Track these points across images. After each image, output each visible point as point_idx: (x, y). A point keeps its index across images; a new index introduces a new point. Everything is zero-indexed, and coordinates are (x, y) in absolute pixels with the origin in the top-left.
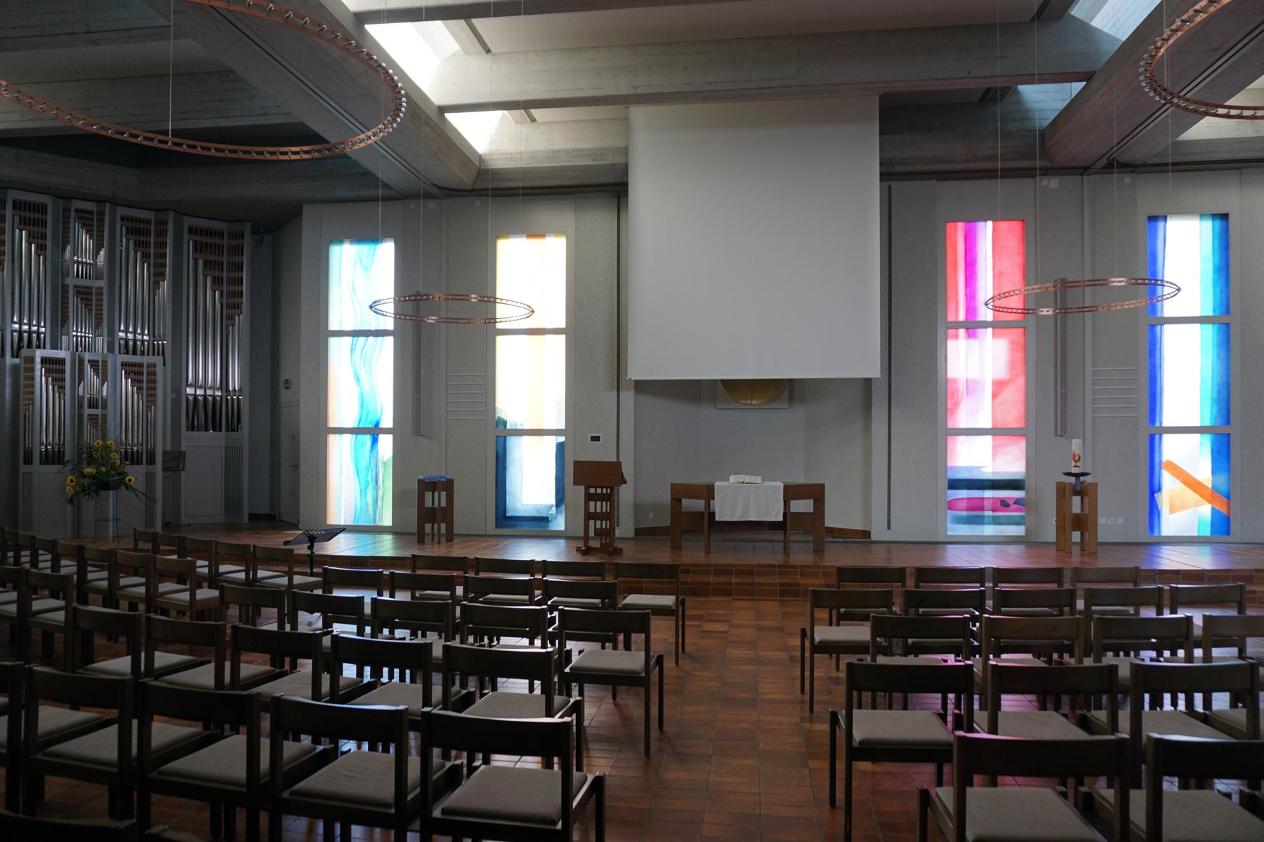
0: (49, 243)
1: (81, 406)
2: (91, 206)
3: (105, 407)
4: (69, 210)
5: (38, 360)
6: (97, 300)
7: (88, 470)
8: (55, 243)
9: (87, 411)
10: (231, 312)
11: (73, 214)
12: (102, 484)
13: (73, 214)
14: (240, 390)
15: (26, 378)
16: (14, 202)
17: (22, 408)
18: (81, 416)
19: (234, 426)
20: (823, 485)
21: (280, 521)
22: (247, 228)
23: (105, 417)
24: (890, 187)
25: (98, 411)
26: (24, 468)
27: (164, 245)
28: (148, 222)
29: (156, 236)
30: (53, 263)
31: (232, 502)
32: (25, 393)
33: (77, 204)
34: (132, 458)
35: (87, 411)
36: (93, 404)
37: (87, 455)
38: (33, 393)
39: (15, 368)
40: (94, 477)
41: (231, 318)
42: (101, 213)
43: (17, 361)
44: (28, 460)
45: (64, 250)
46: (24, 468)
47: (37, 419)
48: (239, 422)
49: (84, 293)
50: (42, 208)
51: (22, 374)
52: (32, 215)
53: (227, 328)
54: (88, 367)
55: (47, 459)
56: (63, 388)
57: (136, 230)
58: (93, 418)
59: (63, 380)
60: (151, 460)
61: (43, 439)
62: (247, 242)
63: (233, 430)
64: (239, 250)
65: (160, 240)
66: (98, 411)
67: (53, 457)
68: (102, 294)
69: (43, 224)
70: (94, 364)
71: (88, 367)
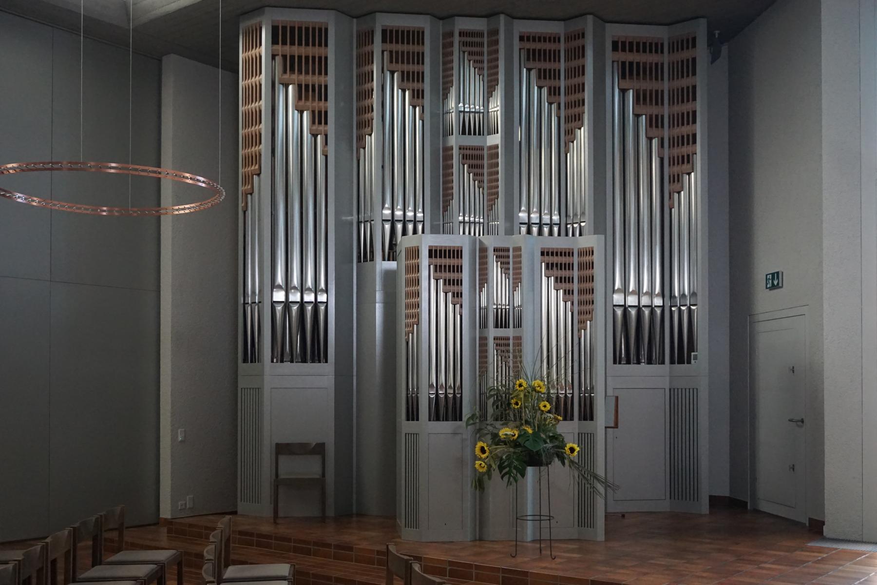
0: (427, 87)
1: (484, 325)
2: (479, 25)
3: (519, 325)
4: (451, 34)
5: (424, 253)
6: (490, 174)
7: (505, 432)
8: (434, 80)
9: (492, 332)
10: (676, 169)
11: (456, 39)
12: (529, 455)
13: (456, 39)
14: (693, 294)
15: (409, 295)
16: (384, 32)
17: (402, 329)
18: (483, 340)
19: (683, 353)
20: (277, 445)
21: (757, 511)
22: (701, 30)
23: (518, 339)
24: (127, 528)
25: (510, 332)
26: (406, 426)
27: (581, 71)
28: (555, 39)
29: (567, 59)
30: (433, 115)
31: (681, 476)
32: (408, 316)
33: (463, 24)
34: (563, 408)
35: (492, 332)
36: (501, 322)
37: (503, 405)
38: (418, 305)
39: (390, 277)
40: (516, 444)
41: (676, 179)
42: (494, 33)
43: (393, 265)
44: (413, 414)
45: (446, 96)
46: (406, 426)
47: (425, 346)
48: (692, 347)
49: (472, 157)
50: (417, 36)
51: (403, 289)
52: (405, 48)
53: (671, 197)
54: (492, 257)
55: (447, 409)
56: (458, 295)
57: (539, 55)
58: (502, 343)
59: (459, 282)
60: (588, 414)
61: (429, 381)
62: (701, 52)
63: (681, 361)
64: (689, 68)
65: (575, 63)
66: (510, 332)
67: (447, 409)
68: (496, 155)
69: (419, 58)
70: (502, 254)
71: (492, 257)
